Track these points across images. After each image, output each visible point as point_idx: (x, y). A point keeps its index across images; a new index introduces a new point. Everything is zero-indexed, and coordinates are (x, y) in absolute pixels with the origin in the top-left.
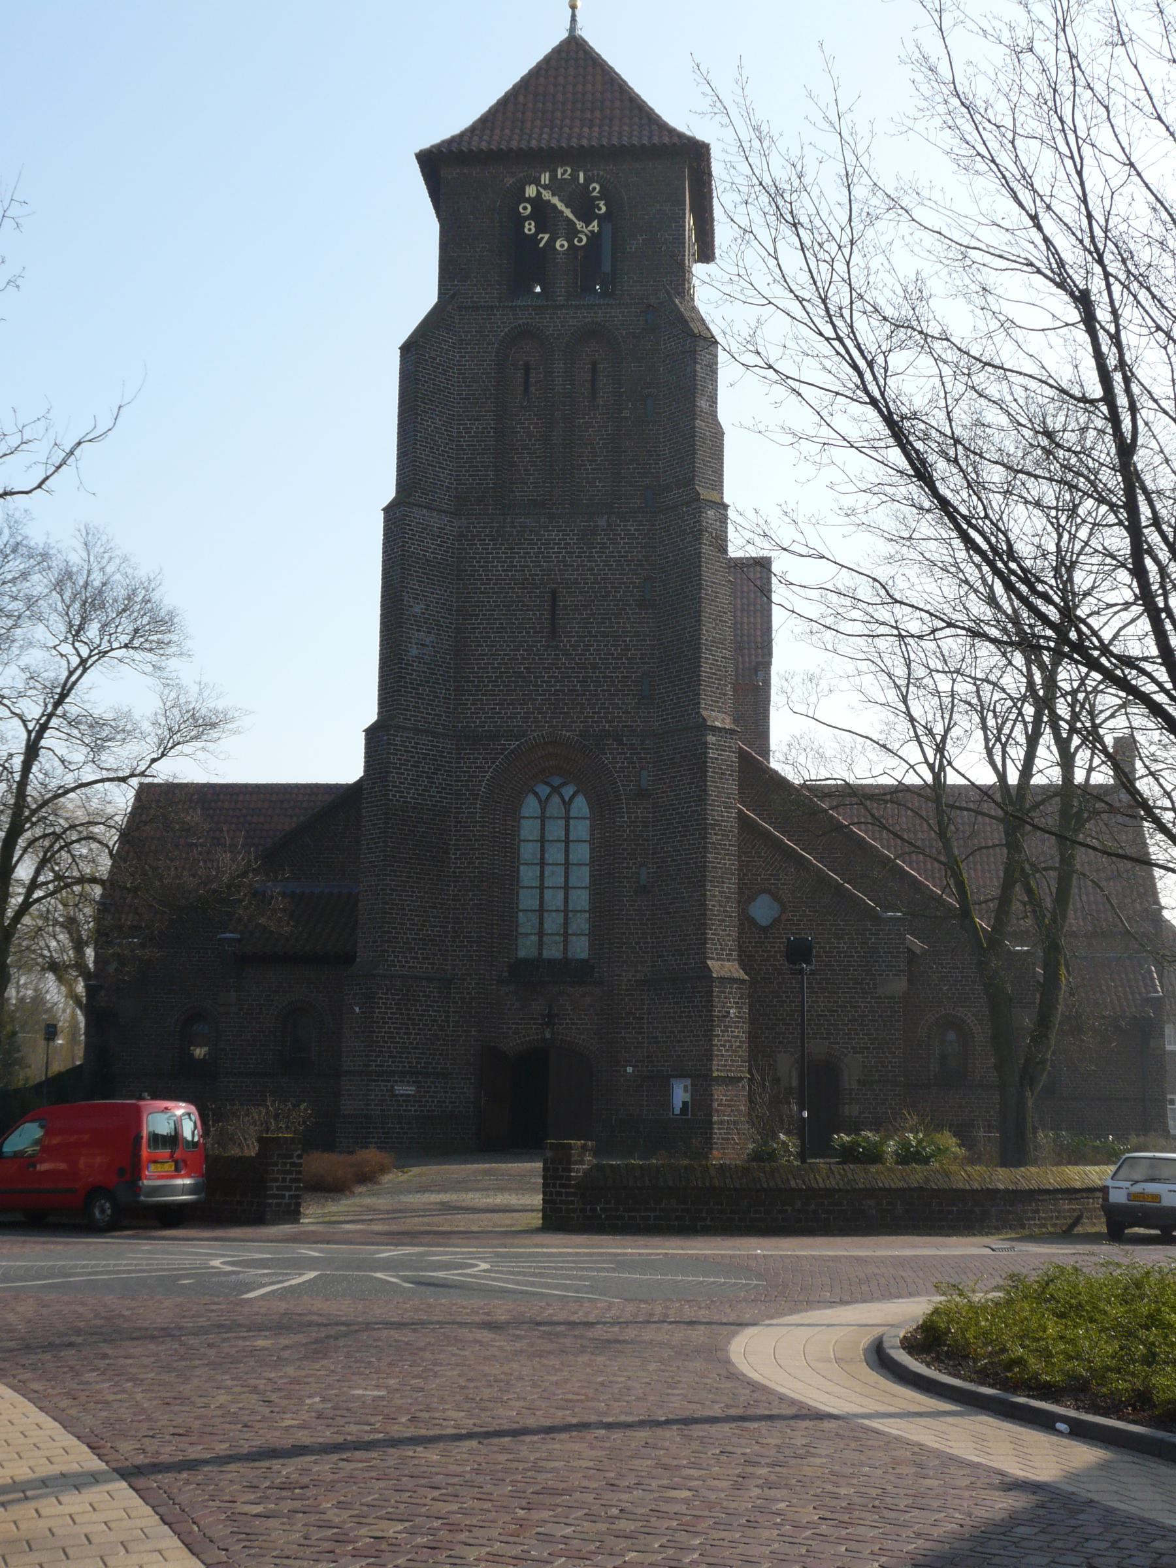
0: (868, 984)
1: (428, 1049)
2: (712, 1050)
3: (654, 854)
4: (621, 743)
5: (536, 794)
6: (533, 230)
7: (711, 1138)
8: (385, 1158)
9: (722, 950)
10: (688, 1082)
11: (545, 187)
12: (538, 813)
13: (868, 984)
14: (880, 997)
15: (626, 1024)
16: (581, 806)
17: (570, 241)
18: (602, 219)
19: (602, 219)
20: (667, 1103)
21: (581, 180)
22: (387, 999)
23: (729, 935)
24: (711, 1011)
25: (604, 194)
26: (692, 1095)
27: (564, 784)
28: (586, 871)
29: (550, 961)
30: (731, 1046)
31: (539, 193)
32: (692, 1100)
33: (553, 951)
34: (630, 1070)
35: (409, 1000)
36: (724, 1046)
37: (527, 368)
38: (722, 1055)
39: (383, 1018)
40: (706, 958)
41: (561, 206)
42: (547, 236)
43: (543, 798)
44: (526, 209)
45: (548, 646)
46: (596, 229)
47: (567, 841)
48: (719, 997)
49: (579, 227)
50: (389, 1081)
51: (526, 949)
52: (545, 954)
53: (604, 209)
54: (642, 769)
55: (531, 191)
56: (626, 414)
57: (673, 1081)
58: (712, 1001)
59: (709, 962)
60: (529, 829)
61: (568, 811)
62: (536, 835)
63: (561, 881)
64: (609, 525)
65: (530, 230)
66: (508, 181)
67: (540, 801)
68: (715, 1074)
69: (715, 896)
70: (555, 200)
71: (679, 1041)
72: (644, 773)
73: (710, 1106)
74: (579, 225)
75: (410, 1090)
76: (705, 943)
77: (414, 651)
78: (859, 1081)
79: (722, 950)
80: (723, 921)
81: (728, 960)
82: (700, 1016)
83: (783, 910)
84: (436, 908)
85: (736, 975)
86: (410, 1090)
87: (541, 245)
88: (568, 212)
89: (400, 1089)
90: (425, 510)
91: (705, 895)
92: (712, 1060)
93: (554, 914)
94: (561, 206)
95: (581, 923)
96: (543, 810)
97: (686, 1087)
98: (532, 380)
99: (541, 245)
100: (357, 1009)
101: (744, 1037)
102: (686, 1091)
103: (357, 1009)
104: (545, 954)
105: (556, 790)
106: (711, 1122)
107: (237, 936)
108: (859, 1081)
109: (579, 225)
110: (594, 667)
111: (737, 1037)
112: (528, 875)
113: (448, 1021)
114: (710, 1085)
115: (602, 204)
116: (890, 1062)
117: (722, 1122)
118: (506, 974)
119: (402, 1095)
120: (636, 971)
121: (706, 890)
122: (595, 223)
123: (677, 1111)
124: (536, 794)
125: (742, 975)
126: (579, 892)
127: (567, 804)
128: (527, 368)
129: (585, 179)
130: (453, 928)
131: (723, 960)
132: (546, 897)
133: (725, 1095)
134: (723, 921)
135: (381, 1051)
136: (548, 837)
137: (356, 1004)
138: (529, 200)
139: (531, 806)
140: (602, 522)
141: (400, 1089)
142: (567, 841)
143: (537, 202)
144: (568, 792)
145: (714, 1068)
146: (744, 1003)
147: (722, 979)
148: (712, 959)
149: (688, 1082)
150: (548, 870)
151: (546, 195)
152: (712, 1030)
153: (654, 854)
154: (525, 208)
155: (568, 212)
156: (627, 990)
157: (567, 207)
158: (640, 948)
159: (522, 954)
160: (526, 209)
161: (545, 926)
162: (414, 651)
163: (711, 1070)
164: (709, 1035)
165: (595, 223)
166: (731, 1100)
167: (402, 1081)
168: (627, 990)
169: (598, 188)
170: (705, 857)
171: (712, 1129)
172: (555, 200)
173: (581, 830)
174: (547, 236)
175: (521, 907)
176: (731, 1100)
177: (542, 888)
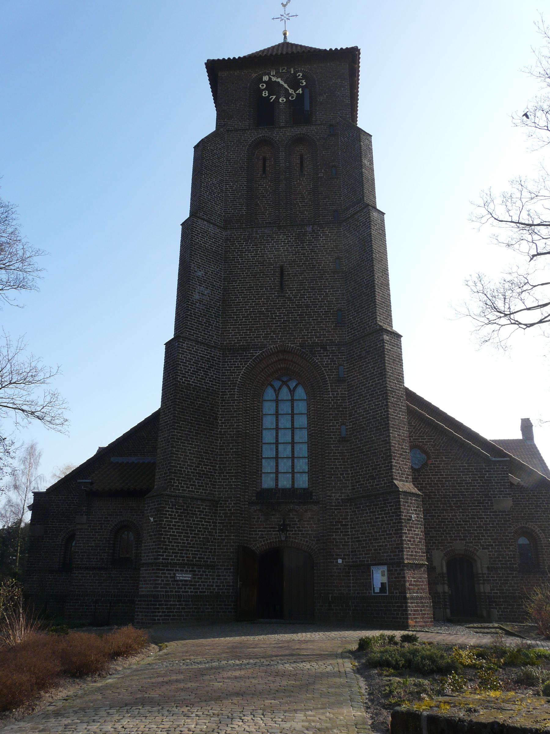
0: (487, 503)
1: (201, 548)
2: (402, 544)
3: (350, 416)
4: (325, 349)
5: (272, 386)
6: (267, 95)
7: (407, 610)
8: (142, 634)
9: (402, 474)
10: (385, 568)
11: (273, 76)
12: (274, 397)
13: (487, 503)
14: (496, 512)
15: (336, 529)
16: (300, 393)
17: (287, 98)
18: (303, 88)
19: (303, 88)
20: (369, 585)
21: (292, 72)
22: (173, 512)
23: (406, 465)
24: (400, 515)
25: (304, 77)
26: (388, 578)
27: (291, 379)
28: (305, 432)
29: (283, 490)
30: (414, 541)
31: (270, 78)
32: (389, 582)
33: (285, 482)
34: (340, 561)
35: (188, 513)
36: (410, 541)
37: (264, 160)
38: (409, 548)
39: (169, 525)
40: (393, 479)
41: (283, 83)
42: (274, 97)
43: (277, 389)
44: (263, 86)
45: (279, 296)
46: (301, 92)
47: (293, 414)
48: (404, 506)
49: (290, 92)
50: (173, 570)
51: (268, 482)
52: (280, 486)
53: (305, 83)
54: (340, 365)
55: (266, 78)
56: (321, 175)
57: (372, 568)
58: (400, 508)
59: (395, 482)
60: (268, 408)
61: (292, 396)
62: (273, 411)
63: (289, 439)
64: (313, 231)
65: (265, 95)
66: (254, 75)
67: (275, 391)
68: (406, 562)
69: (395, 437)
70: (279, 80)
71: (376, 539)
72: (341, 368)
73: (404, 585)
74: (291, 91)
75: (188, 577)
76: (392, 469)
77: (197, 297)
78: (488, 568)
79: (402, 474)
80: (402, 454)
81: (407, 481)
82: (392, 520)
83: (429, 458)
84: (208, 453)
85: (413, 491)
86: (188, 577)
87: (272, 101)
88: (286, 86)
89: (180, 576)
90: (205, 223)
91: (389, 436)
92: (403, 551)
93: (285, 460)
94: (282, 82)
95: (302, 465)
96: (277, 396)
97: (383, 573)
98: (267, 165)
99: (272, 101)
100: (152, 519)
101: (422, 535)
102: (383, 575)
103: (152, 519)
104: (280, 486)
105: (285, 383)
106: (405, 598)
107: (90, 481)
108: (488, 568)
109: (291, 91)
110: (308, 306)
111: (417, 535)
112: (268, 437)
113: (216, 529)
114: (403, 570)
115: (303, 81)
116: (508, 555)
117: (412, 598)
118: (254, 498)
119: (181, 581)
120: (341, 493)
121: (389, 433)
122: (300, 89)
123: (377, 590)
124: (272, 386)
125: (415, 490)
126: (301, 446)
127: (292, 392)
128: (264, 160)
129: (294, 72)
130: (219, 467)
131: (403, 481)
132: (279, 449)
133: (413, 578)
134: (402, 454)
135: (166, 549)
136: (280, 412)
137: (151, 516)
138: (265, 82)
139: (270, 394)
140: (309, 229)
141: (180, 576)
142: (293, 414)
143: (270, 83)
144: (292, 384)
145: (405, 557)
146: (420, 511)
147: (405, 493)
148: (397, 479)
149: (385, 568)
150: (281, 433)
151: (274, 79)
152: (402, 529)
153: (350, 416)
154: (263, 86)
155: (286, 86)
156: (336, 506)
157: (285, 83)
158: (344, 477)
159: (265, 486)
160: (263, 86)
161: (280, 468)
162: (197, 297)
163: (403, 559)
164: (399, 533)
165: (300, 89)
166: (417, 581)
167: (182, 571)
168: (336, 506)
169: (301, 75)
170: (388, 411)
171: (406, 603)
172: (279, 80)
173: (302, 407)
174: (274, 97)
175: (263, 471)
176: (417, 581)
177: (277, 443)
